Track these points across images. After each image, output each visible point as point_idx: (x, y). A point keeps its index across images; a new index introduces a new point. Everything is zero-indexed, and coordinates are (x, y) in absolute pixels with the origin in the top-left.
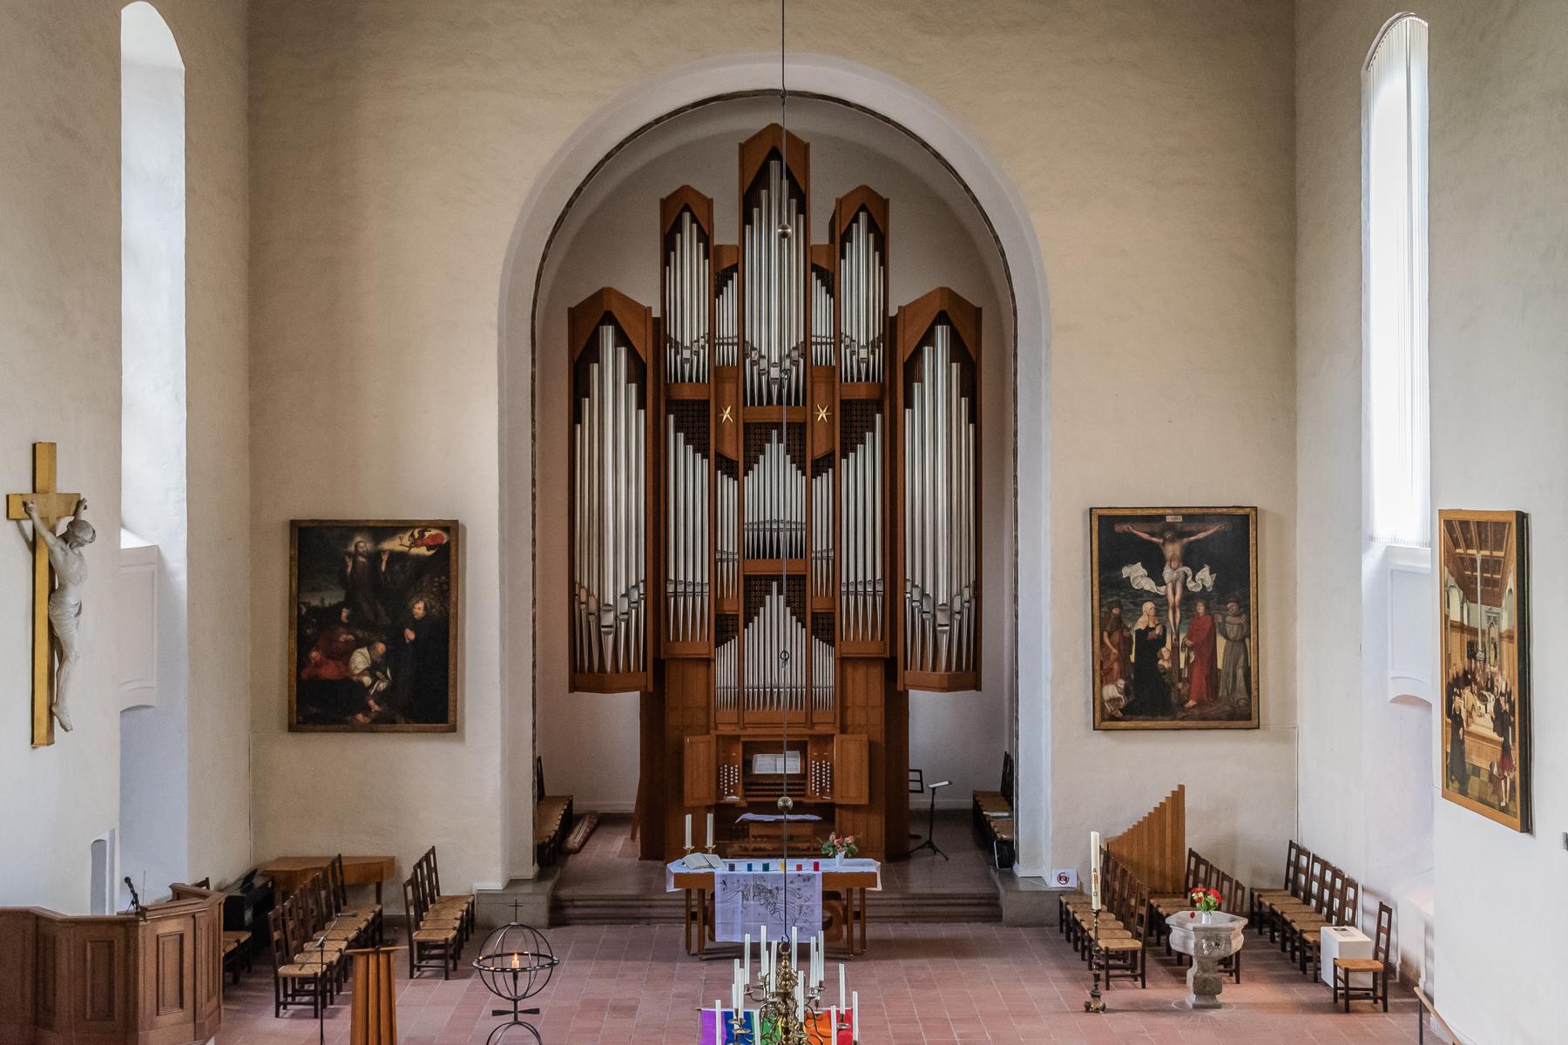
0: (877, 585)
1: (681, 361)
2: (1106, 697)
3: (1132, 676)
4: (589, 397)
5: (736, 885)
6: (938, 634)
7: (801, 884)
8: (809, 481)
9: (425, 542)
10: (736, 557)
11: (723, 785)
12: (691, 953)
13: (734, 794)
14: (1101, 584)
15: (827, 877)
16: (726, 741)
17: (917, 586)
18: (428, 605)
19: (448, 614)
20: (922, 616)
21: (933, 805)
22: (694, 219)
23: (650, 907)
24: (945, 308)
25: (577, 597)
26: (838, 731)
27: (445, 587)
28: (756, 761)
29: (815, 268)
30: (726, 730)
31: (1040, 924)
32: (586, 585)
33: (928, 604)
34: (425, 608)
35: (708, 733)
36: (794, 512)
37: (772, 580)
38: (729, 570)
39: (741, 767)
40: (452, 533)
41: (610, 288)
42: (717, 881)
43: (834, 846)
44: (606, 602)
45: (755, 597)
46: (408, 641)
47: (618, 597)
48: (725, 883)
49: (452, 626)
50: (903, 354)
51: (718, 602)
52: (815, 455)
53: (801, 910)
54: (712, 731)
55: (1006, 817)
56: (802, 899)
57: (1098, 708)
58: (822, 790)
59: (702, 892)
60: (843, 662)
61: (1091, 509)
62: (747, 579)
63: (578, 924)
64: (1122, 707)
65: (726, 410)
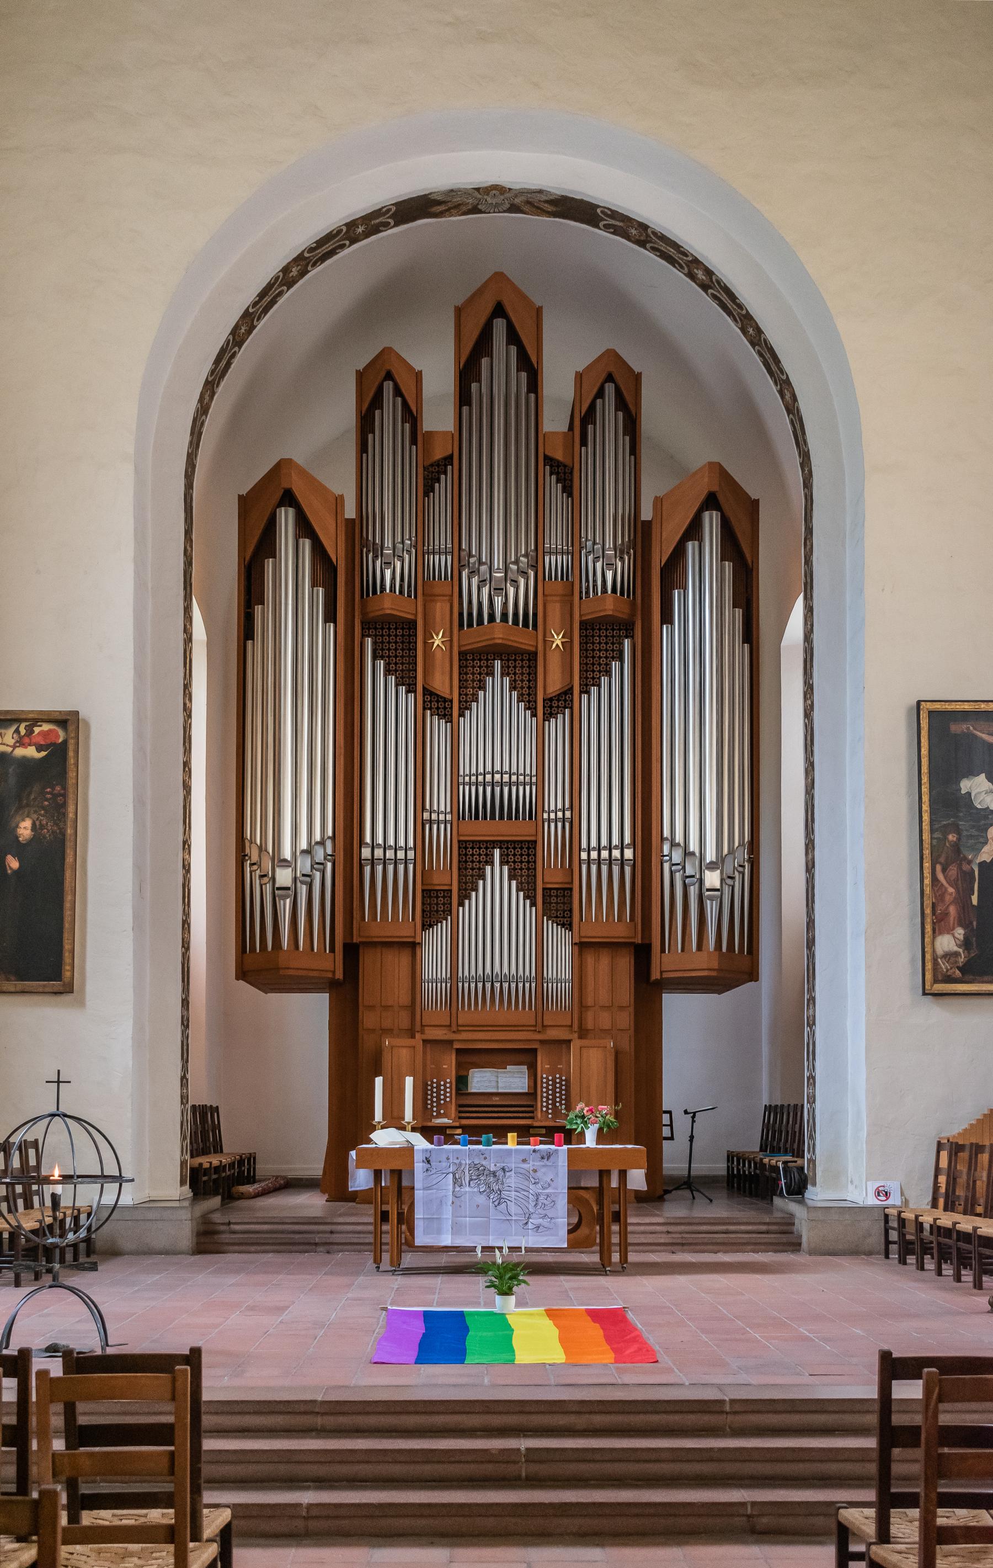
2: (940, 951)
3: (975, 923)
9: (34, 740)
13: (445, 1116)
17: (678, 845)
18: (38, 823)
23: (332, 1232)
24: (715, 488)
26: (576, 1035)
28: (473, 1077)
29: (548, 460)
31: (854, 1252)
33: (694, 865)
34: (34, 828)
35: (413, 1037)
36: (525, 763)
37: (494, 848)
38: (441, 836)
40: (71, 728)
42: (418, 1157)
46: (9, 872)
47: (298, 853)
48: (429, 1162)
50: (659, 558)
51: (426, 874)
54: (418, 1035)
57: (929, 966)
59: (397, 1174)
60: (582, 947)
64: (961, 965)
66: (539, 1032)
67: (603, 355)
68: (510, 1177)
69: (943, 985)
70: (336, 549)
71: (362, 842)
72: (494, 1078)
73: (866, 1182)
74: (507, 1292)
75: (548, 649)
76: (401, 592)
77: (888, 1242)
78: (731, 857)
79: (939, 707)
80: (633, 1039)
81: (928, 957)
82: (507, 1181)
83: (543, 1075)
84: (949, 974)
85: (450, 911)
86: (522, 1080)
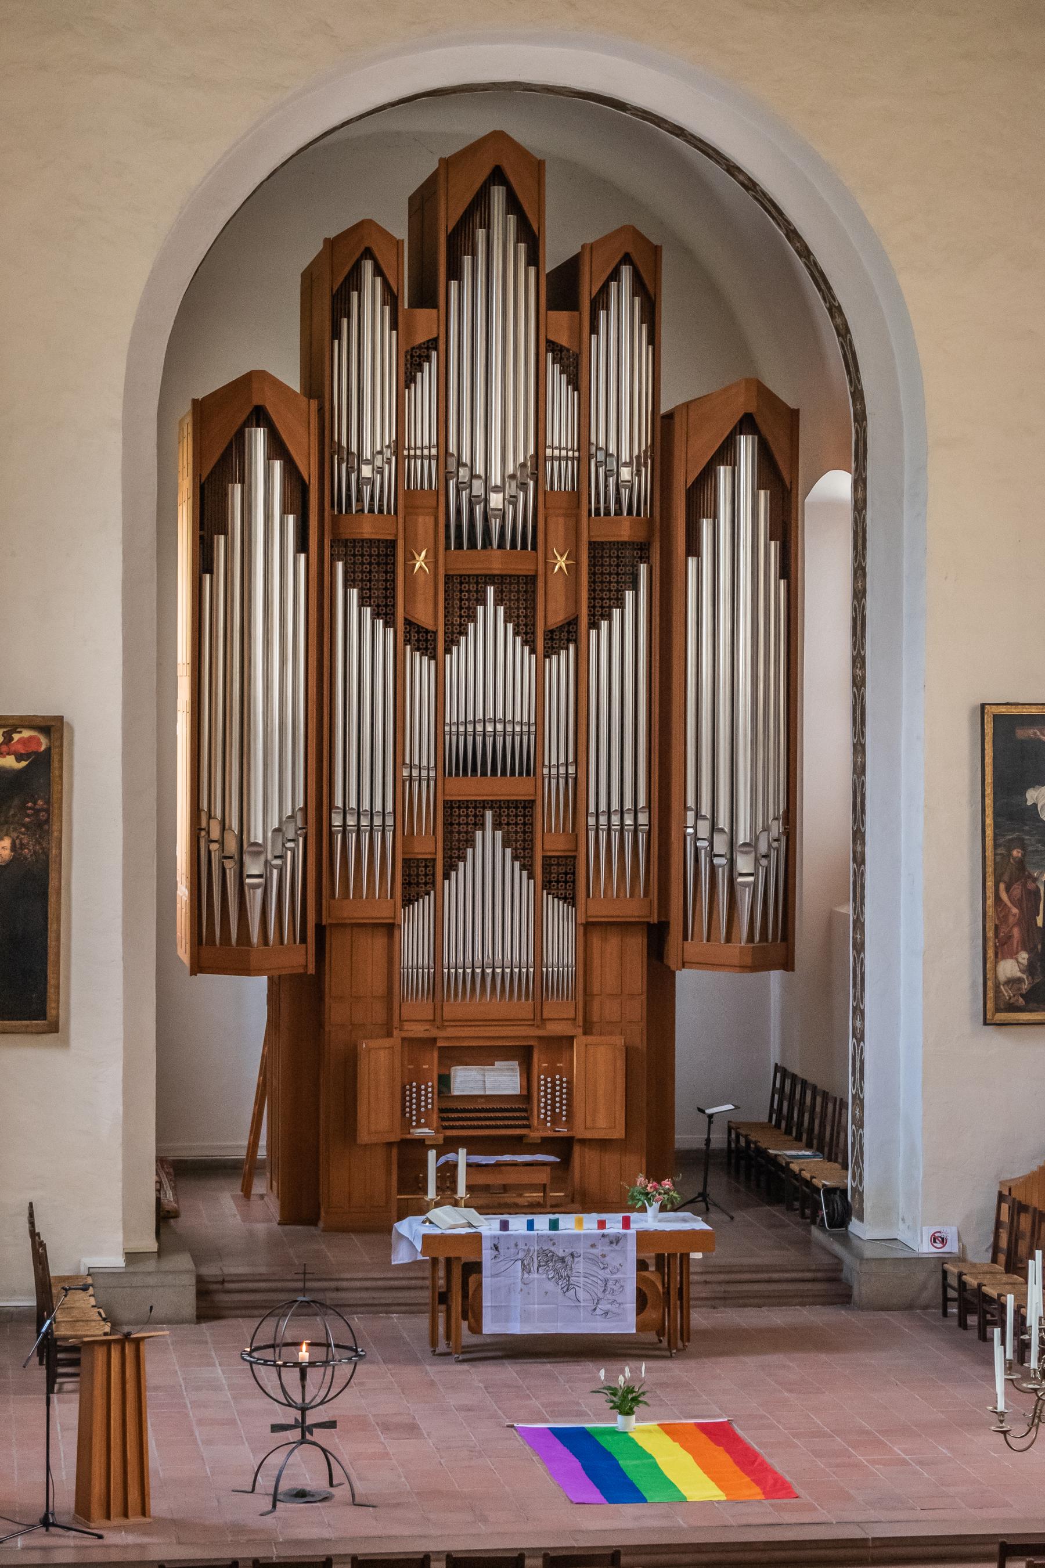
0: (640, 815)
1: (470, 501)
2: (1002, 978)
4: (226, 534)
5: (513, 1250)
6: (738, 888)
7: (607, 1249)
8: (540, 662)
9: (13, 749)
10: (432, 773)
11: (410, 1113)
12: (437, 1352)
13: (425, 1125)
14: (996, 814)
15: (644, 1238)
16: (417, 1045)
17: (704, 818)
18: (17, 842)
19: (48, 856)
20: (712, 861)
21: (708, 1141)
22: (378, 271)
23: (337, 1290)
24: (752, 409)
25: (203, 833)
26: (580, 1030)
27: (43, 815)
28: (455, 1076)
29: (553, 346)
30: (418, 1030)
31: (908, 1307)
32: (219, 814)
35: (389, 1034)
38: (423, 794)
39: (436, 1087)
40: (55, 735)
41: (263, 372)
42: (486, 1245)
43: (647, 1194)
44: (252, 840)
45: (459, 832)
48: (497, 1248)
49: (53, 875)
50: (682, 480)
52: (549, 624)
53: (606, 1285)
54: (396, 1033)
55: (808, 1157)
56: (608, 1271)
57: (991, 994)
58: (555, 1120)
60: (588, 928)
61: (983, 706)
62: (449, 805)
63: (237, 1317)
64: (1024, 992)
65: (420, 555)
66: (538, 1027)
67: (619, 231)
68: (578, 1262)
69: (1006, 1014)
70: (308, 469)
71: (331, 806)
72: (480, 1078)
73: (921, 1228)
74: (629, 1413)
75: (549, 573)
76: (381, 511)
77: (946, 1300)
78: (766, 833)
79: (1004, 710)
80: (645, 1032)
81: (990, 984)
82: (576, 1267)
83: (541, 1080)
84: (1012, 1001)
85: (434, 883)
86: (514, 1079)
